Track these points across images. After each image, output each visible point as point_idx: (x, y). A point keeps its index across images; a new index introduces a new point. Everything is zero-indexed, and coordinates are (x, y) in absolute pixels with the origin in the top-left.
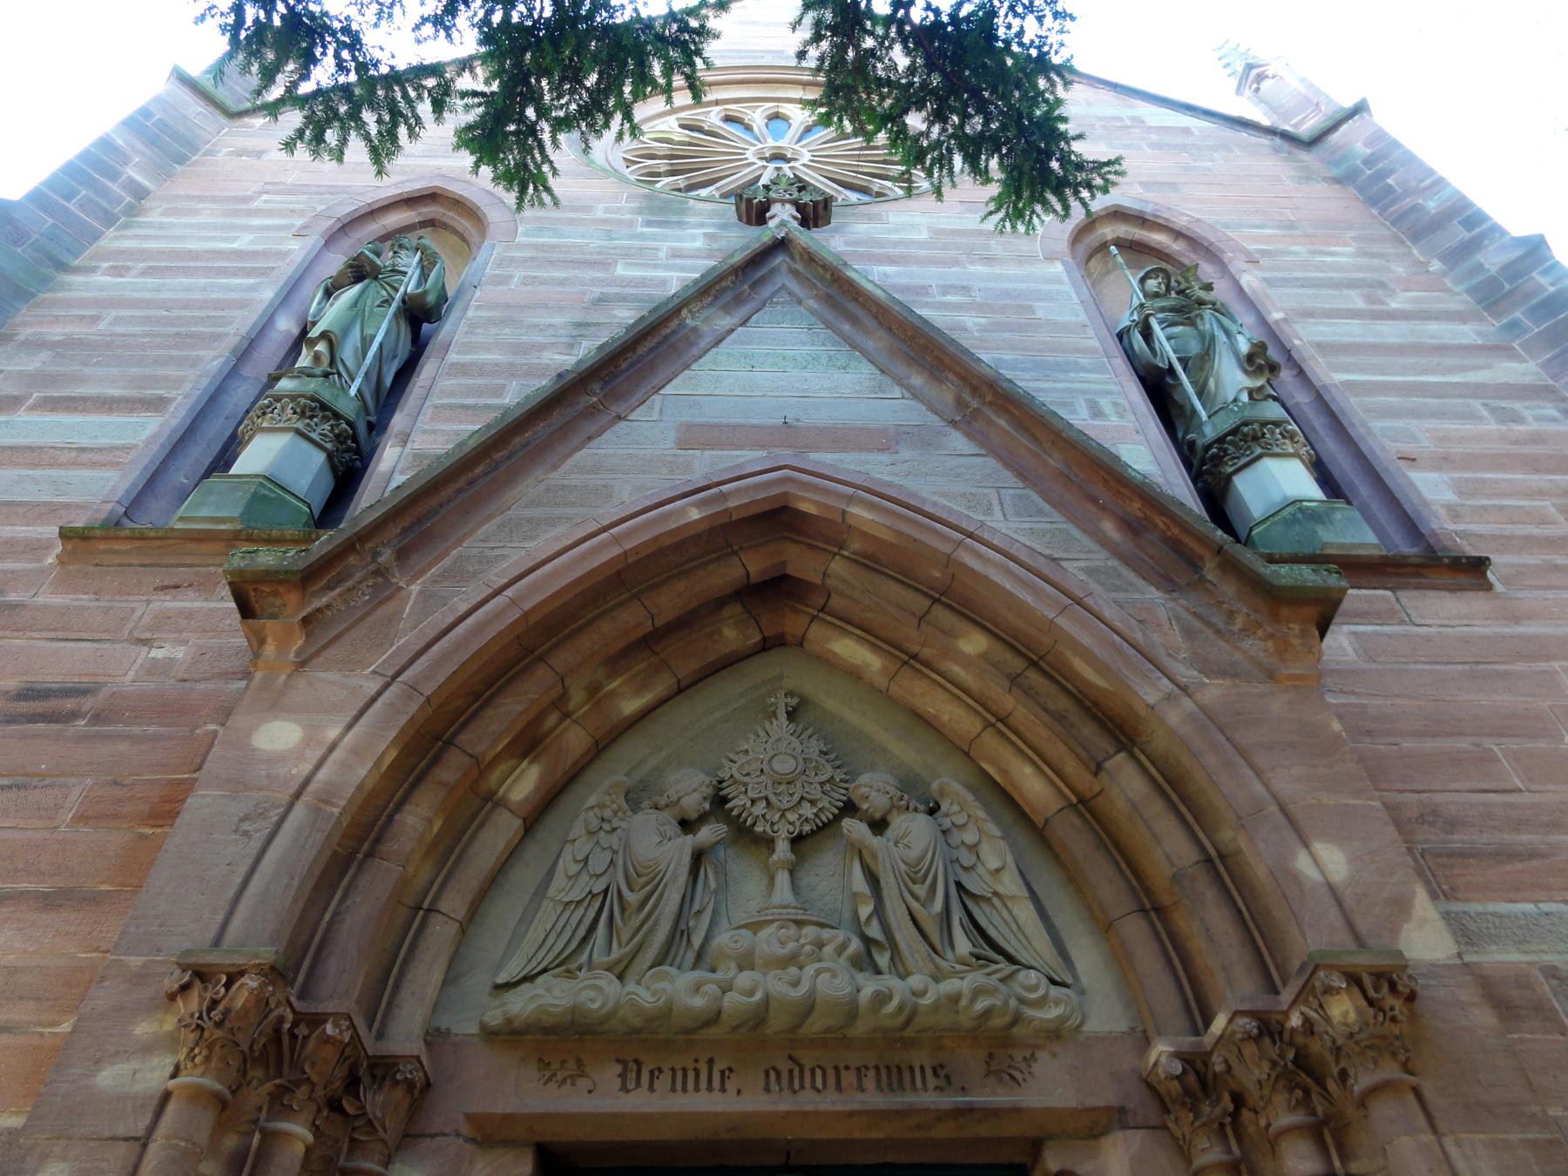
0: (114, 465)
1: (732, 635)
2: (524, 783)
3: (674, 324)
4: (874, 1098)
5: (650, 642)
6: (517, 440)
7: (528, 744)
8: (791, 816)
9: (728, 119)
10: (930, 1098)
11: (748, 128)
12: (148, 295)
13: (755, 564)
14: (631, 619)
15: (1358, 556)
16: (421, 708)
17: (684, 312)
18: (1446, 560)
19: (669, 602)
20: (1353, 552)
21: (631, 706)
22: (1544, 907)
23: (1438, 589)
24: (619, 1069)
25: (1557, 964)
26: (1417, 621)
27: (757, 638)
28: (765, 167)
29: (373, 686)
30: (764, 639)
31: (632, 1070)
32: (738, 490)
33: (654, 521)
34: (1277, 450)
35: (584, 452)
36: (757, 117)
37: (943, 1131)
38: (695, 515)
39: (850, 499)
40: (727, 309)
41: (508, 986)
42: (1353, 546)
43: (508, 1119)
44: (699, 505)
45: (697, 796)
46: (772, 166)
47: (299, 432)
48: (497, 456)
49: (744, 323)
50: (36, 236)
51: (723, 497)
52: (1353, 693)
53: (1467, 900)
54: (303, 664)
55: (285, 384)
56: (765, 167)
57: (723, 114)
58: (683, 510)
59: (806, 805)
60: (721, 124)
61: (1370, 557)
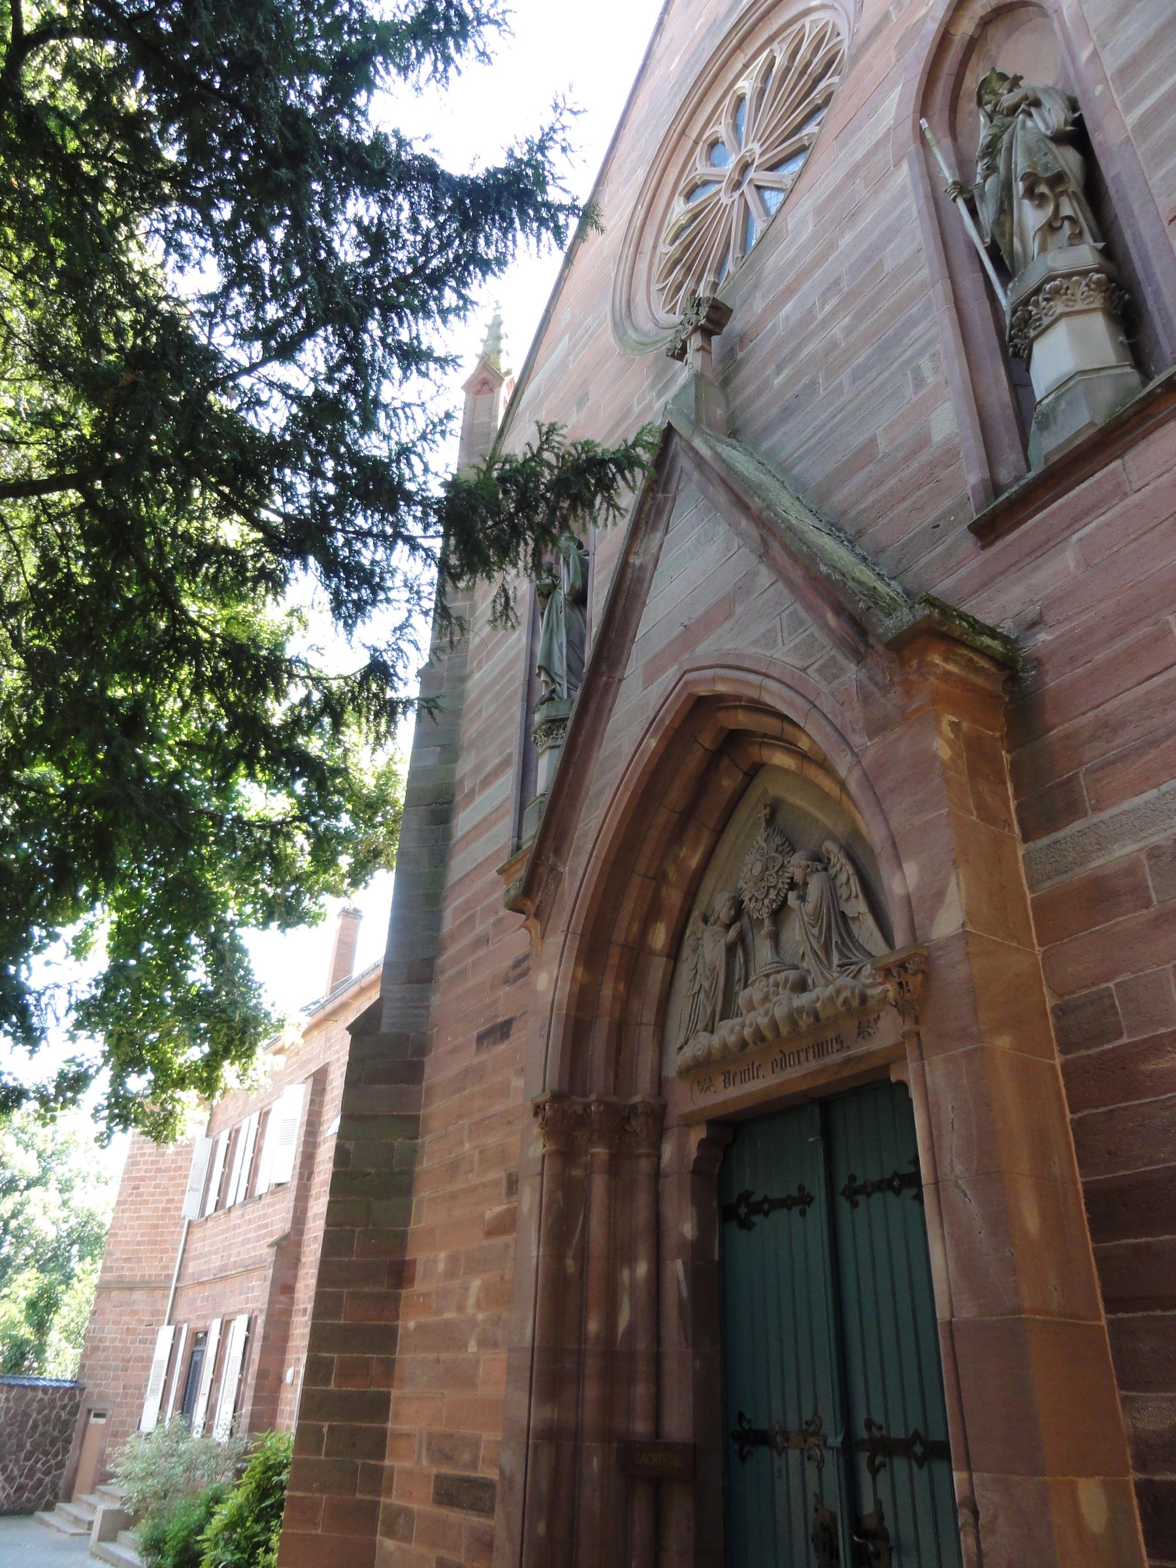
0: (503, 816)
1: (728, 783)
2: (659, 937)
3: (629, 575)
4: (813, 1065)
5: (688, 815)
6: (581, 739)
7: (649, 919)
8: (766, 902)
9: (689, 196)
10: (835, 1058)
11: (706, 183)
12: (504, 664)
13: (707, 740)
14: (662, 818)
15: (1079, 446)
16: (581, 940)
17: (632, 559)
18: (1159, 390)
19: (676, 796)
20: (1072, 447)
21: (694, 862)
22: (1164, 788)
23: (1163, 425)
24: (722, 1078)
25: (1160, 843)
26: (1136, 486)
27: (740, 776)
28: (742, 194)
29: (562, 939)
30: (745, 774)
31: (729, 1079)
32: (667, 710)
33: (634, 770)
34: (1046, 321)
35: (611, 720)
36: (701, 169)
37: (846, 1073)
38: (653, 743)
39: (714, 680)
40: (654, 529)
41: (681, 1048)
42: (1069, 441)
43: (692, 1114)
44: (652, 736)
45: (725, 910)
46: (745, 187)
47: (551, 747)
48: (575, 759)
49: (666, 533)
50: (445, 674)
51: (662, 720)
52: (1068, 619)
53: (1108, 806)
54: (543, 937)
55: (537, 718)
56: (742, 194)
57: (682, 199)
58: (647, 743)
59: (772, 890)
60: (691, 205)
61: (1088, 439)
